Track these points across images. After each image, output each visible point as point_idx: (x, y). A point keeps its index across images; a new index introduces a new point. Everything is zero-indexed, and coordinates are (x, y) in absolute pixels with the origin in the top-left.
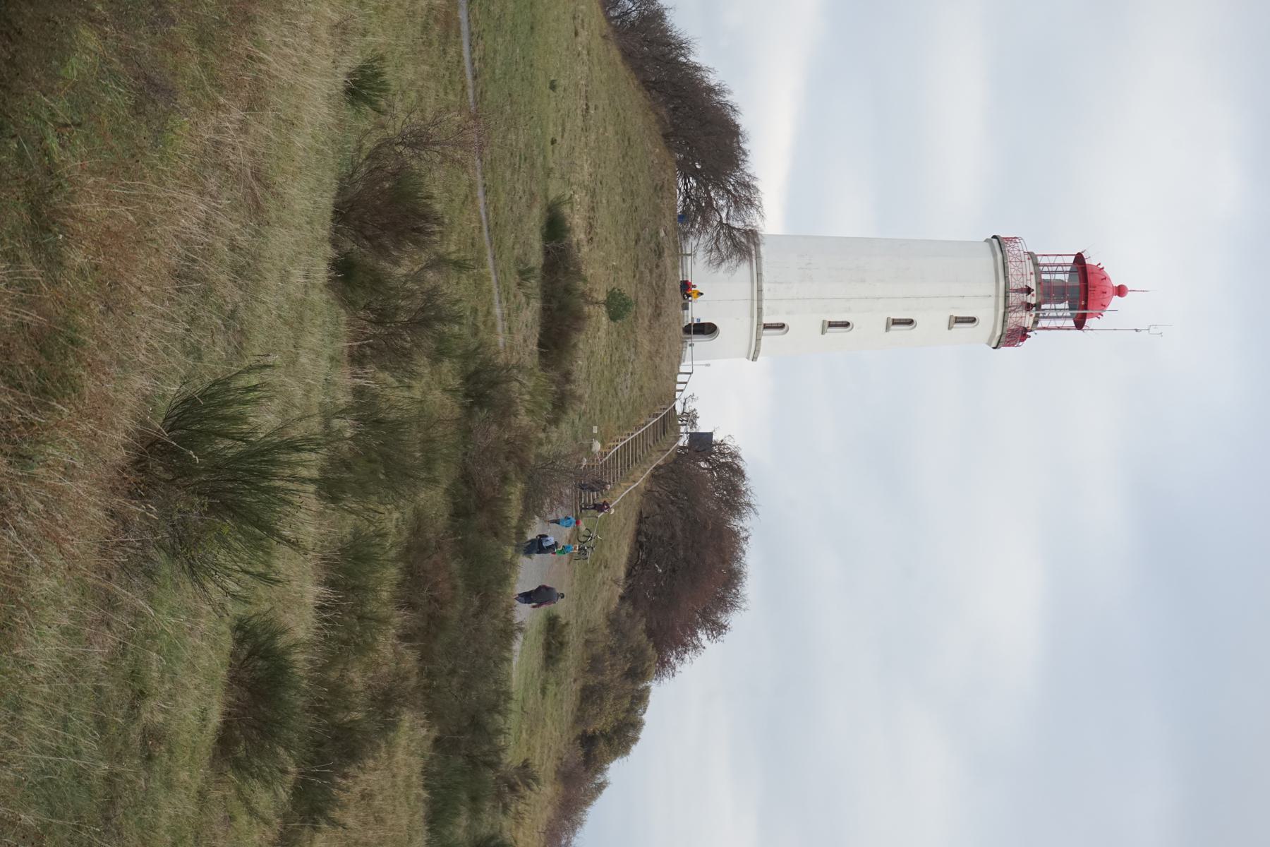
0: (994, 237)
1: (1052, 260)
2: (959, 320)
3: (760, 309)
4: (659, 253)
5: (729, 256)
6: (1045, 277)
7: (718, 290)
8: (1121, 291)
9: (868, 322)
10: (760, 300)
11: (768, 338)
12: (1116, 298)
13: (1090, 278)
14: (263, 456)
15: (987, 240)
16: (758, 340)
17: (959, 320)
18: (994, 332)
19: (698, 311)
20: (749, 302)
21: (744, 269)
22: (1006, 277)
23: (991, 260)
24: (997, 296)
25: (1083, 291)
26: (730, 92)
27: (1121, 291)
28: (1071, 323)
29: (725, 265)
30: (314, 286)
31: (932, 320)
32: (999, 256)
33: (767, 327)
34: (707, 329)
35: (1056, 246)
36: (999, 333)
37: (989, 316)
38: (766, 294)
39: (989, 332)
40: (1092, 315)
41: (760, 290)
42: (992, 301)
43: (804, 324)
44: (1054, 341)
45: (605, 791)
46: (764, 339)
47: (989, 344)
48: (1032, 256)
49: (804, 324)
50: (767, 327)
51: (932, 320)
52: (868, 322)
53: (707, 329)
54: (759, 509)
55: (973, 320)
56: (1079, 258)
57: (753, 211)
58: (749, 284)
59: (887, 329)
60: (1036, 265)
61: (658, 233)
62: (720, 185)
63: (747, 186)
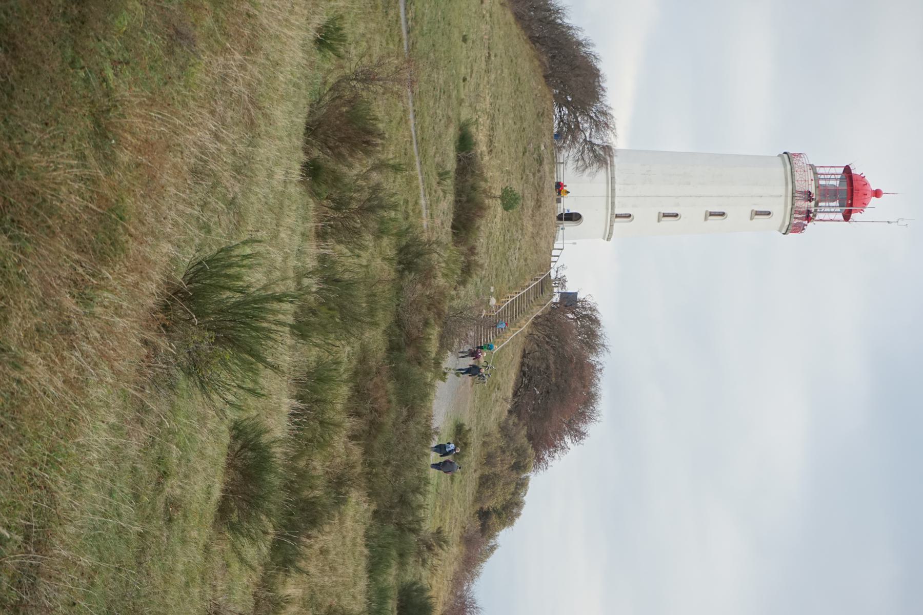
0: (785, 153)
2: (759, 213)
3: (613, 203)
4: (540, 161)
5: (591, 164)
7: (582, 189)
8: (877, 193)
9: (692, 213)
10: (613, 197)
11: (619, 224)
12: (874, 199)
13: (855, 184)
15: (779, 155)
16: (611, 226)
17: (759, 213)
18: (784, 222)
19: (568, 205)
20: (605, 199)
21: (602, 175)
22: (793, 182)
24: (786, 196)
25: (851, 192)
27: (877, 193)
29: (588, 171)
30: (291, 182)
31: (738, 213)
32: (789, 167)
33: (617, 216)
35: (829, 160)
36: (787, 223)
39: (780, 221)
40: (856, 211)
41: (613, 190)
42: (782, 199)
43: (645, 214)
44: (828, 228)
46: (616, 225)
47: (780, 231)
48: (813, 167)
49: (645, 214)
50: (617, 216)
51: (738, 213)
52: (692, 213)
53: (573, 217)
54: (610, 349)
55: (769, 213)
56: (847, 170)
57: (609, 132)
58: (605, 211)
59: (706, 219)
60: (815, 173)
61: (539, 147)
62: (585, 112)
63: (604, 114)
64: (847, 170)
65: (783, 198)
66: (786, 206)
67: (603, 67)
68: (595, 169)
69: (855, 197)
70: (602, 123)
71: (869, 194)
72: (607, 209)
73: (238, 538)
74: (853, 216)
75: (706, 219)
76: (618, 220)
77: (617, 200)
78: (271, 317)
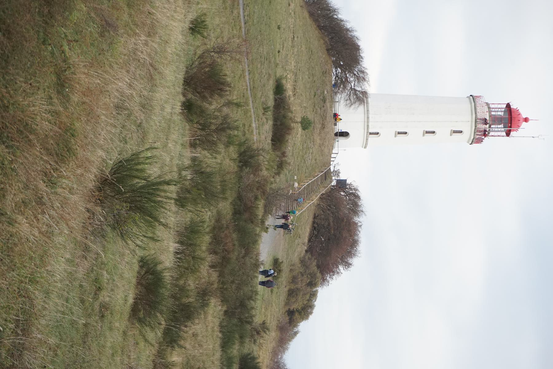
1: (496, 106)
2: (455, 132)
3: (368, 126)
4: (324, 101)
5: (355, 103)
8: (526, 120)
9: (415, 132)
10: (368, 122)
12: (524, 123)
13: (513, 114)
16: (367, 139)
19: (341, 127)
21: (361, 108)
23: (470, 105)
24: (472, 122)
25: (510, 119)
26: (356, 31)
27: (526, 120)
28: (504, 134)
29: (353, 107)
31: (443, 131)
33: (370, 134)
34: (344, 134)
35: (498, 101)
38: (371, 119)
40: (514, 130)
41: (368, 118)
42: (470, 123)
44: (496, 141)
46: (369, 139)
50: (370, 134)
51: (443, 131)
52: (415, 132)
53: (344, 134)
56: (508, 106)
57: (365, 83)
59: (424, 135)
60: (489, 108)
62: (351, 71)
63: (363, 72)
64: (508, 106)
67: (362, 44)
69: (513, 122)
70: (361, 77)
71: (521, 120)
74: (512, 133)
75: (479, 136)
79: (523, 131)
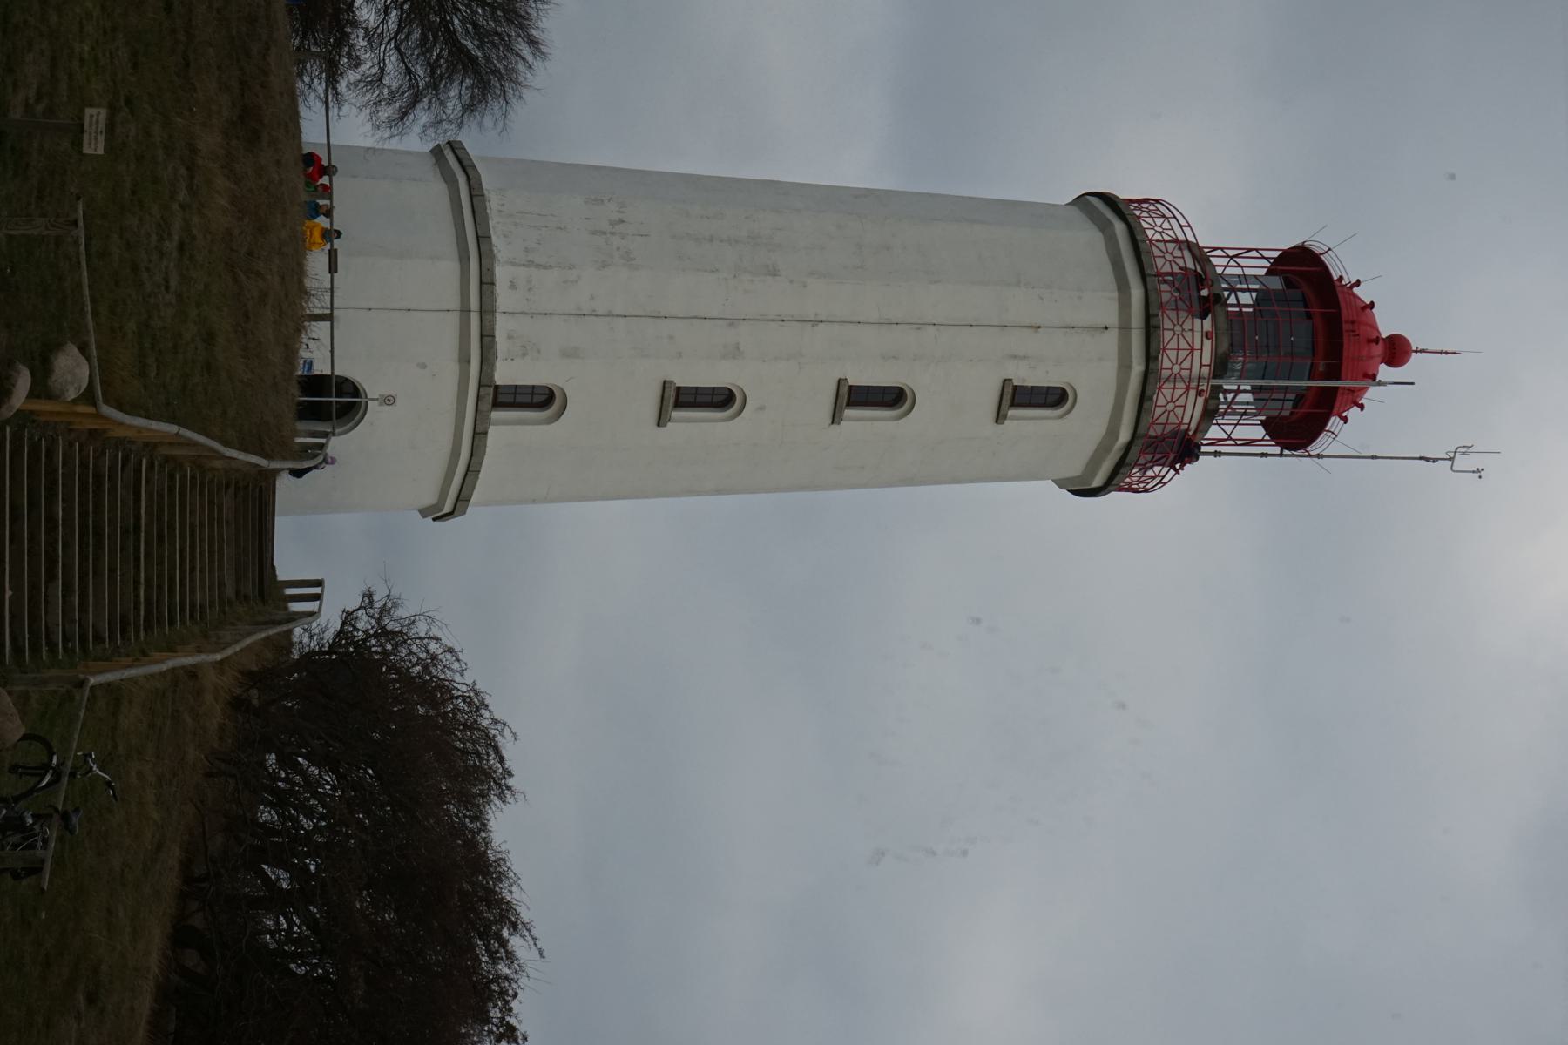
0: (1106, 198)
6: (1205, 370)
8: (1397, 350)
9: (786, 390)
10: (487, 310)
11: (509, 433)
14: (146, 630)
15: (1081, 201)
16: (479, 435)
17: (1019, 397)
18: (1112, 432)
20: (454, 319)
24: (1125, 328)
28: (1172, 472)
31: (954, 391)
35: (1234, 215)
36: (1124, 436)
37: (1096, 374)
38: (504, 298)
39: (1099, 428)
41: (487, 283)
43: (609, 392)
45: (1343, 265)
51: (954, 391)
52: (786, 390)
55: (1055, 398)
59: (836, 417)
65: (1112, 338)
66: (1124, 366)
68: (453, 106)
72: (465, 360)
73: (390, 101)
75: (836, 417)
76: (496, 415)
77: (502, 326)
78: (1186, 420)
79: (1380, 415)
